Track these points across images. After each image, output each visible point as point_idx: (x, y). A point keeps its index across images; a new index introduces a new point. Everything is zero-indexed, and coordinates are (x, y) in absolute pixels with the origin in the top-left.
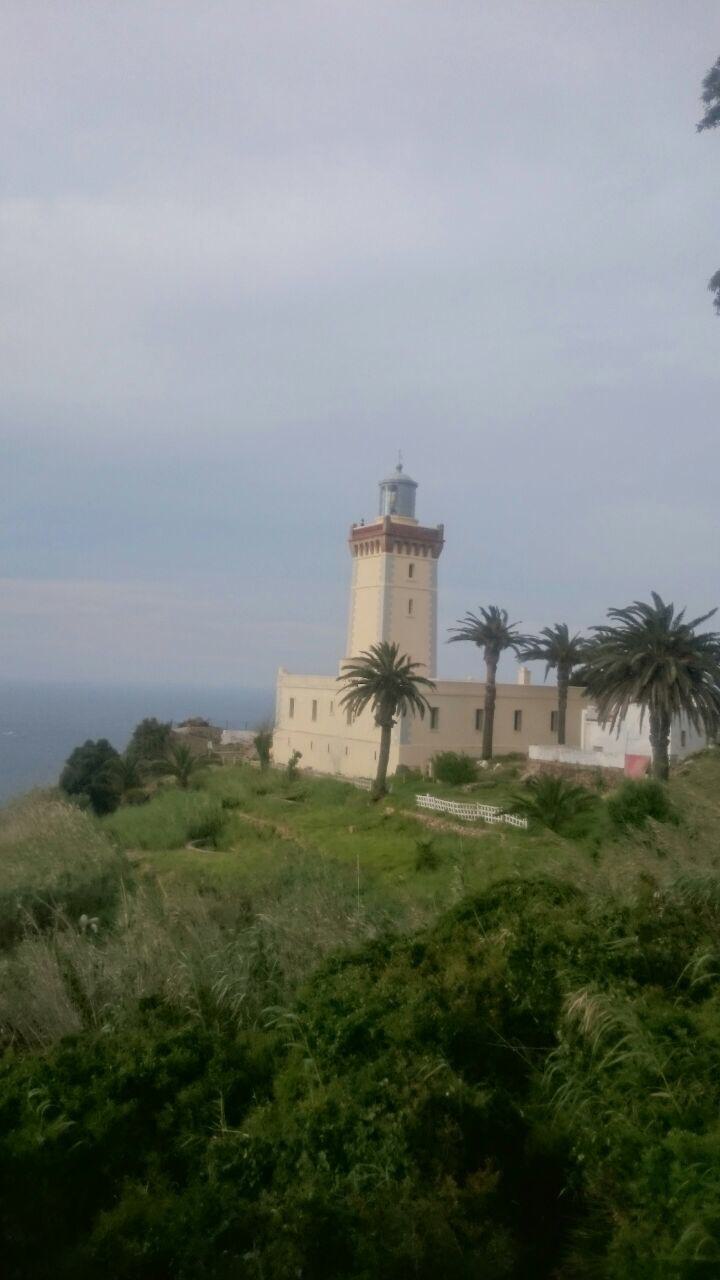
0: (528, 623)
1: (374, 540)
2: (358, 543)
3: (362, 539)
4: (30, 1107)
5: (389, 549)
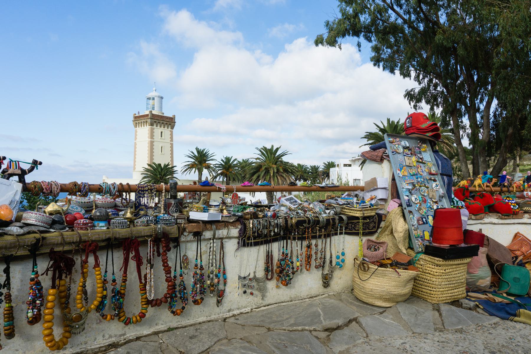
0: (217, 158)
1: (145, 121)
2: (137, 122)
3: (138, 119)
4: (414, 232)
5: (152, 125)
